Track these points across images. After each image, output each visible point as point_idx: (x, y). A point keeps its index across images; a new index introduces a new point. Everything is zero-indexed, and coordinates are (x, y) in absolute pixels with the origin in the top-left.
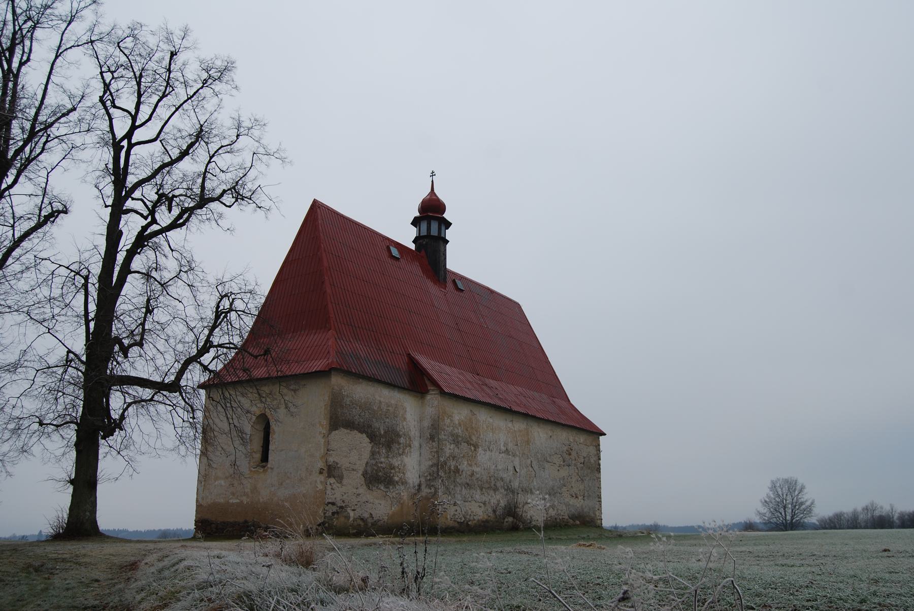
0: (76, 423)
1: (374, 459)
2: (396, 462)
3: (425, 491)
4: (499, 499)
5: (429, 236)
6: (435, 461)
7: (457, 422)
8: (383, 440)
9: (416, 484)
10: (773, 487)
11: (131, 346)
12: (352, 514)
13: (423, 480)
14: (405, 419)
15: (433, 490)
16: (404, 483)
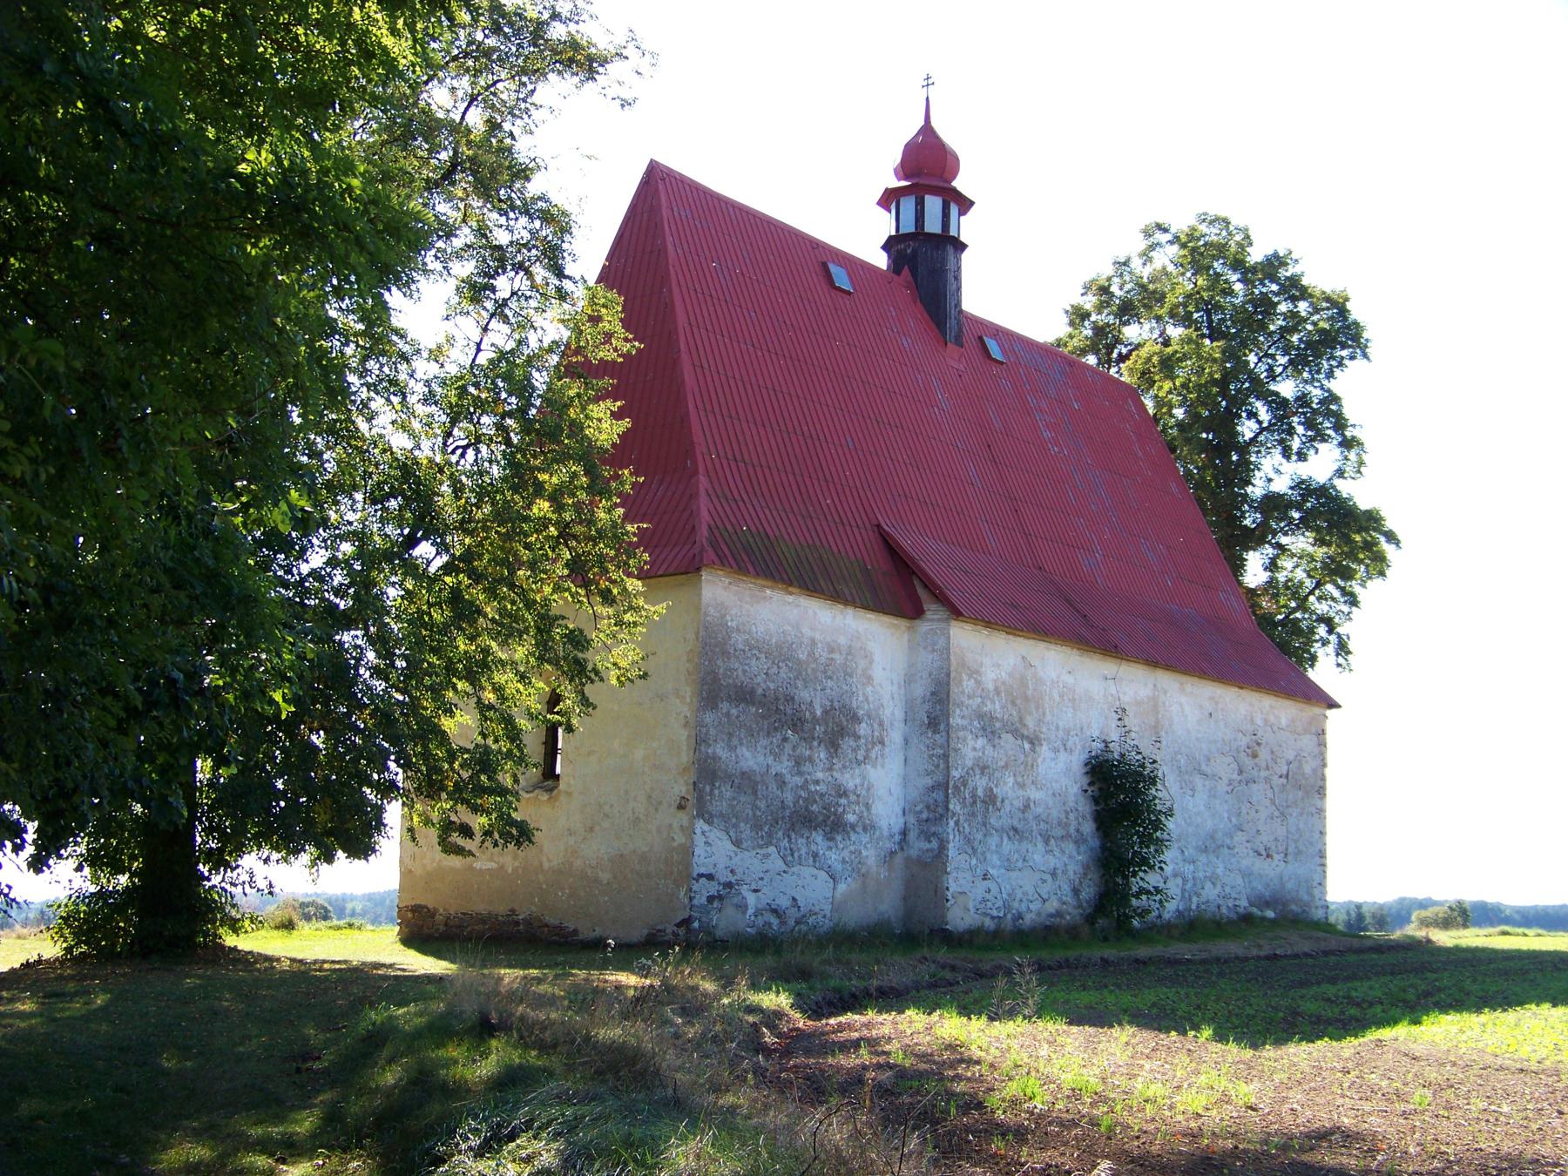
1: (800, 773)
2: (849, 780)
3: (918, 846)
5: (919, 235)
6: (940, 778)
7: (991, 686)
12: (751, 899)
13: (912, 820)
14: (870, 678)
15: (935, 844)
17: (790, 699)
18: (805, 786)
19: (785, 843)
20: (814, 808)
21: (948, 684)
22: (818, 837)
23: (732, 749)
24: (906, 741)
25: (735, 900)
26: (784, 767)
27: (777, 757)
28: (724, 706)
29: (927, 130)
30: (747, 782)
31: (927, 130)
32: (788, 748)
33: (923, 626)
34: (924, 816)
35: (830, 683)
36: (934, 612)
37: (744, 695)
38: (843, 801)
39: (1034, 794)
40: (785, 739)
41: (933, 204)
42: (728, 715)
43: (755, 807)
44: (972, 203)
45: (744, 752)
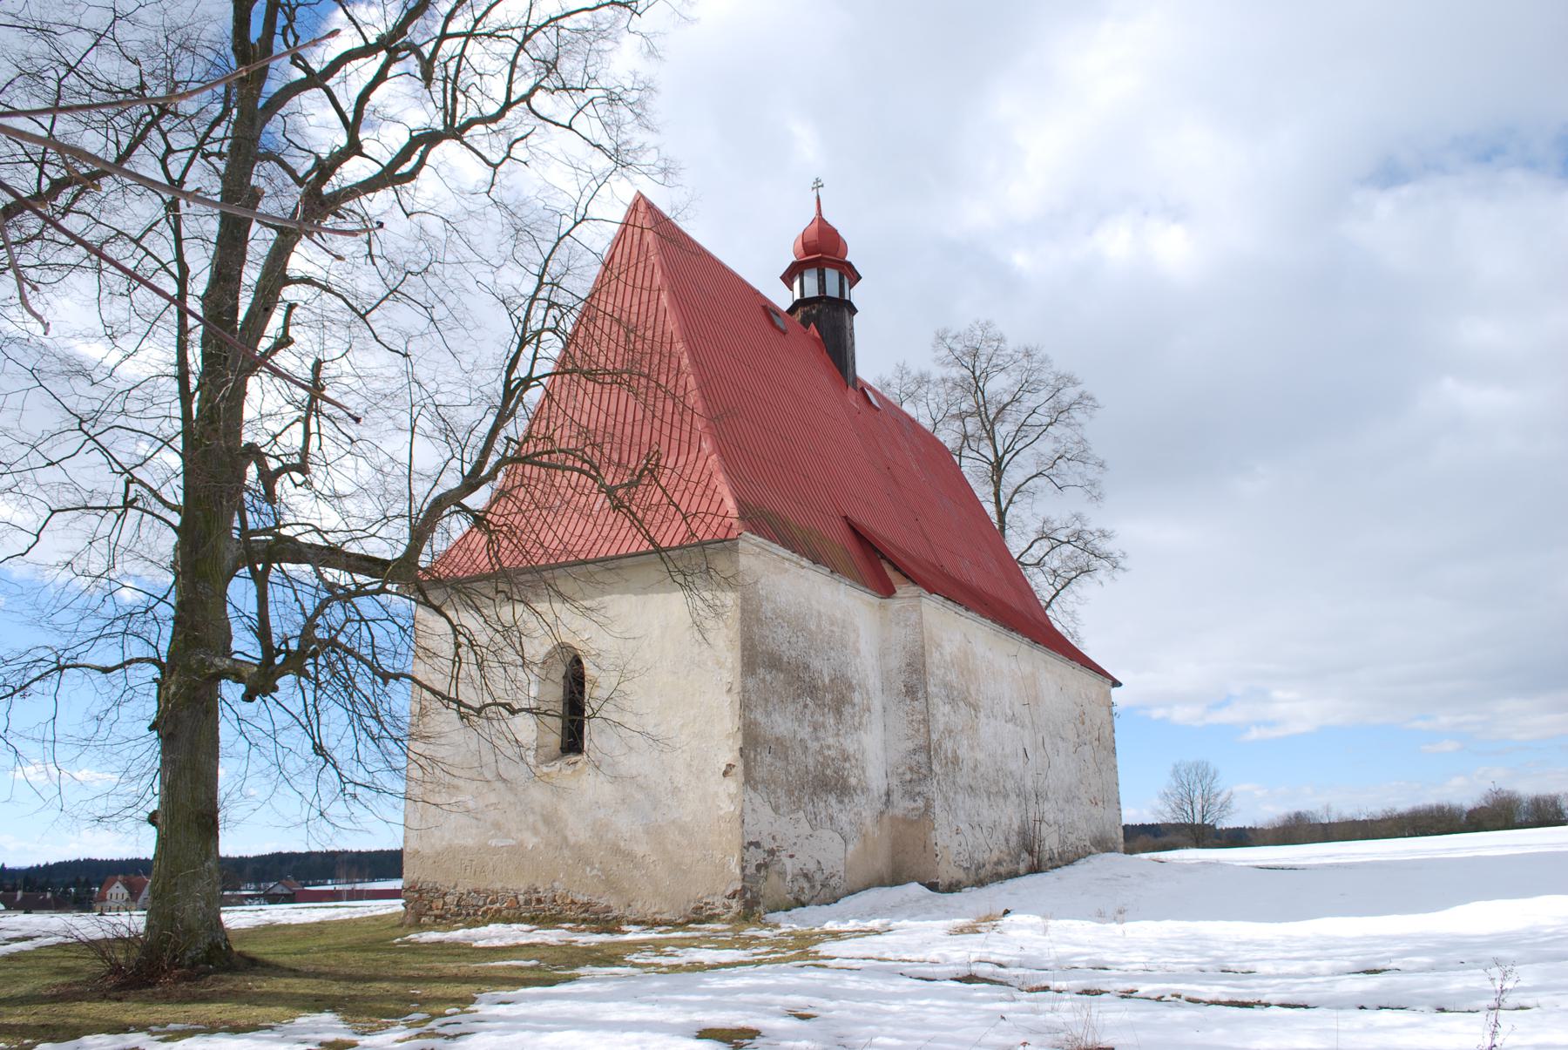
0: (156, 661)
1: (817, 739)
2: (851, 747)
3: (902, 806)
4: (1009, 816)
5: (822, 299)
6: (921, 741)
7: (948, 658)
8: (829, 697)
9: (883, 792)
10: (1176, 772)
11: (279, 472)
12: (788, 862)
13: (895, 781)
14: (858, 651)
15: (920, 803)
16: (866, 790)
17: (807, 667)
18: (820, 752)
19: (810, 807)
20: (829, 772)
21: (923, 655)
22: (832, 800)
23: (768, 714)
24: (885, 709)
25: (777, 867)
26: (805, 732)
27: (800, 721)
28: (761, 671)
29: (820, 220)
30: (780, 748)
31: (820, 220)
32: (808, 712)
33: (894, 604)
34: (908, 777)
35: (833, 654)
36: (905, 590)
37: (774, 663)
38: (847, 765)
39: (980, 756)
40: (806, 706)
41: (832, 276)
42: (764, 680)
43: (788, 773)
44: (859, 278)
45: (776, 717)
